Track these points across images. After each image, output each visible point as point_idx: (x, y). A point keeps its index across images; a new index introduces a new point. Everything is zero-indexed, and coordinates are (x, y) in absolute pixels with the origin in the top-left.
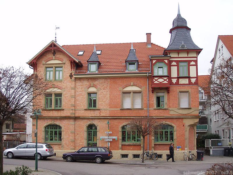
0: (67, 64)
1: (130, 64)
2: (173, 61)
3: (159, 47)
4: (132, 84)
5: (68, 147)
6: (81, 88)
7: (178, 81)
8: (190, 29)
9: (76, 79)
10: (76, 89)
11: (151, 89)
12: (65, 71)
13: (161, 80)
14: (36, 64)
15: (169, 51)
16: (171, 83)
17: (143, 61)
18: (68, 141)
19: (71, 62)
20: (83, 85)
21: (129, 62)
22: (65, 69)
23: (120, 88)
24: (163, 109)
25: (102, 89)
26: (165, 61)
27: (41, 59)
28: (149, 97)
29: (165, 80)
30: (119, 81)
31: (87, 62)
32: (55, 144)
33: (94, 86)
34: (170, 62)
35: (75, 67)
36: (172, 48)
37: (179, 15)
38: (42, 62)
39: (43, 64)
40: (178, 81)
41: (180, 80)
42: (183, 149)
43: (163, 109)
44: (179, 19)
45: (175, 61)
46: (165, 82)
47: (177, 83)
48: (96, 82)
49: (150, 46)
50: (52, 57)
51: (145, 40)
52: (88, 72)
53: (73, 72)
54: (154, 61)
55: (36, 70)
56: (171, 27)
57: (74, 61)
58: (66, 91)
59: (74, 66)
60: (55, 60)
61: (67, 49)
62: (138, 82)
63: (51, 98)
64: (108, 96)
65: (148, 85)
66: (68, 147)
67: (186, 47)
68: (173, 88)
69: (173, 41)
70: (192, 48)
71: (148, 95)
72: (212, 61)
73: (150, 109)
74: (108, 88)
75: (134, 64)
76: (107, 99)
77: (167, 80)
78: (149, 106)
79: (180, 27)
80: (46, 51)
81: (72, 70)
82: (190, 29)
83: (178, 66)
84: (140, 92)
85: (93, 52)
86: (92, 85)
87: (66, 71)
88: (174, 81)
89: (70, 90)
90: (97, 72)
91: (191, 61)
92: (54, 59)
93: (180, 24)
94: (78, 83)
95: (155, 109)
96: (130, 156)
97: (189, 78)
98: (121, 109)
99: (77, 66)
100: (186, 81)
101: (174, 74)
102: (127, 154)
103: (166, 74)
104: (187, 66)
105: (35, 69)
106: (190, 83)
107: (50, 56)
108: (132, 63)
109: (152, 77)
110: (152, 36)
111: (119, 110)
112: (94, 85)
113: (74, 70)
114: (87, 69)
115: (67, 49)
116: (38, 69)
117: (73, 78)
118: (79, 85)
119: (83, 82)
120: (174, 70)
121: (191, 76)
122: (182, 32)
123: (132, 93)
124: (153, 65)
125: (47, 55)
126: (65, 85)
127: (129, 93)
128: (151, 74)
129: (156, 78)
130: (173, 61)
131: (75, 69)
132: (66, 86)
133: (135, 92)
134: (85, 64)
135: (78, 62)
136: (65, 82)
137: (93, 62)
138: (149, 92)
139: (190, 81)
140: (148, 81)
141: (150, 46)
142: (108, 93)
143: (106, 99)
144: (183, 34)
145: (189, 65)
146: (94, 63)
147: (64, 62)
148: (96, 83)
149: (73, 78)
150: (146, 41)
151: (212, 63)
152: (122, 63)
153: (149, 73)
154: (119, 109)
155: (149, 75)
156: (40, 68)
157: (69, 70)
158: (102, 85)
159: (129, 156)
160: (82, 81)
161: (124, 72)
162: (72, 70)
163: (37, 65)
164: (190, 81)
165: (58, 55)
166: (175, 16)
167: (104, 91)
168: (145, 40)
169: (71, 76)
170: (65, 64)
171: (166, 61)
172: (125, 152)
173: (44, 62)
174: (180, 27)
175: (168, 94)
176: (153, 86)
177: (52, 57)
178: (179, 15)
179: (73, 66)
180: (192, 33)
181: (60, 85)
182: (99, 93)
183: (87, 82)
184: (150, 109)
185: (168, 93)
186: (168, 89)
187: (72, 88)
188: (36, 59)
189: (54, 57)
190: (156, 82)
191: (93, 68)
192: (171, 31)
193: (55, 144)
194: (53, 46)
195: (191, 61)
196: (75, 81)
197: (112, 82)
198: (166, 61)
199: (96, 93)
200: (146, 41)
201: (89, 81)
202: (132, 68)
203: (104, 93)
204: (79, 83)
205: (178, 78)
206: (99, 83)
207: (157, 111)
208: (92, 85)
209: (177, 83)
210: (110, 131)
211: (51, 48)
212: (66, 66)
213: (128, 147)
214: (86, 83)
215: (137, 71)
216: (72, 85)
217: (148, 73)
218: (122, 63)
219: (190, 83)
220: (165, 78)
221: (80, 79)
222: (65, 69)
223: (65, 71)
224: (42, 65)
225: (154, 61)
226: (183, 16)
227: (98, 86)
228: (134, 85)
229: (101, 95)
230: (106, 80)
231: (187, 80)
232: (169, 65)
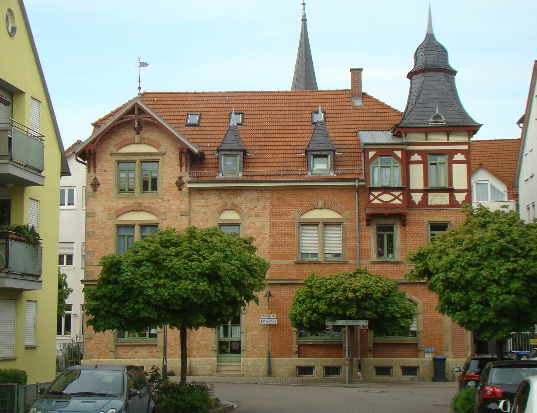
0: (315, 304)
1: (315, 156)
2: (413, 152)
3: (383, 104)
4: (321, 203)
5: (173, 352)
6: (202, 211)
7: (425, 199)
8: (454, 73)
9: (192, 192)
10: (192, 214)
11: (363, 216)
12: (164, 170)
13: (386, 197)
14: (95, 153)
15: (406, 130)
16: (409, 203)
17: (345, 147)
18: (174, 337)
19: (181, 153)
20: (207, 206)
21: (313, 153)
22: (165, 167)
23: (294, 214)
24: (392, 263)
25: (252, 214)
26: (396, 155)
27: (107, 141)
28: (360, 235)
29: (396, 198)
30: (290, 197)
31: (218, 151)
32: (141, 346)
33: (234, 208)
34: (408, 154)
35: (189, 163)
36: (411, 122)
37: (430, 37)
38: (107, 148)
39: (112, 155)
40: (425, 199)
41: (431, 196)
42: (357, 357)
43: (392, 263)
44: (428, 49)
45: (419, 152)
46: (397, 202)
47: (424, 203)
48: (239, 198)
49: (358, 103)
50: (134, 138)
51: (346, 84)
52: (220, 175)
53: (187, 178)
54: (371, 154)
55: (95, 167)
56: (410, 67)
57: (190, 152)
58: (168, 220)
59: (186, 161)
60: (141, 143)
61: (156, 106)
62: (335, 199)
63: (132, 234)
64: (267, 231)
65: (359, 207)
66: (173, 352)
67: (443, 121)
68: (413, 215)
69: (414, 99)
70: (458, 121)
71: (357, 230)
72: (521, 121)
73: (362, 262)
74: (267, 212)
75: (326, 156)
76: (264, 239)
77: (401, 197)
78: (362, 254)
79: (432, 66)
80: (118, 122)
81: (181, 170)
82: (454, 73)
83: (424, 162)
84: (338, 223)
85: (227, 128)
86: (229, 206)
87: (168, 171)
88: (417, 198)
89: (177, 217)
90: (241, 175)
91: (456, 152)
92: (139, 142)
93: (432, 60)
94: (196, 201)
95: (374, 263)
96: (318, 371)
97: (451, 191)
98: (297, 263)
99: (194, 160)
100: (443, 199)
101: (417, 181)
102: (311, 365)
103: (398, 183)
104: (447, 164)
105: (92, 166)
106: (453, 204)
107: (129, 134)
108: (320, 155)
109: (365, 190)
110: (364, 75)
111: (293, 263)
112: (233, 205)
113: (186, 171)
114: (217, 167)
115: (156, 106)
116: (99, 166)
117: (185, 190)
118: (199, 204)
119: (207, 199)
120: (417, 173)
121: (455, 186)
122: (435, 83)
123: (320, 225)
124: (368, 162)
125: (121, 132)
126: (166, 204)
127: (314, 223)
128: (363, 183)
129: (376, 193)
130: (413, 152)
131: (188, 168)
132: (169, 208)
133: (328, 224)
134: (210, 155)
135: (196, 151)
136: (167, 197)
137: (231, 152)
138: (359, 223)
139: (452, 198)
140: (358, 198)
141: (358, 103)
142: (267, 225)
143: (262, 238)
144: (438, 87)
145: (451, 162)
146: (234, 153)
147: (162, 149)
148: (239, 200)
149: (185, 190)
150: (349, 87)
151: (521, 125)
152: (295, 152)
153: (359, 181)
154: (292, 262)
155: (359, 185)
156: (105, 164)
157: (176, 169)
158: (252, 207)
159: (315, 372)
160: (206, 195)
161: (302, 178)
162: (181, 170)
163: (98, 156)
164: (452, 198)
165: (146, 134)
166: (421, 39)
167: (256, 219)
168: (346, 84)
169: (180, 184)
170: (164, 154)
171: (399, 154)
172: (304, 362)
173: (113, 150)
174: (432, 66)
175: (404, 227)
176: (370, 211)
177: (133, 136)
178: (430, 37)
179: (184, 159)
180: (457, 79)
181: (154, 204)
182: (245, 224)
183: (217, 198)
184: (362, 262)
185: (404, 225)
186: (403, 218)
187: (182, 212)
188: (95, 144)
189: (137, 138)
190: (376, 202)
191: (231, 166)
192: (410, 76)
193: (141, 346)
194: (136, 112)
195: (456, 152)
196: (189, 196)
197: (276, 199)
198: (399, 154)
199: (238, 225)
200: (349, 87)
201: (222, 195)
202: (321, 166)
203: (257, 223)
204: (198, 201)
205: (426, 191)
206: (245, 202)
207: (377, 267)
208: (229, 206)
209: (424, 203)
210: (271, 313)
211: (133, 117)
212: (168, 160)
213: (312, 350)
214: (214, 201)
215: (332, 174)
216: (181, 204)
217: (357, 181)
218: (295, 152)
219: (453, 204)
220: (397, 193)
221: (201, 192)
222: (165, 167)
223: (163, 172)
224: (108, 157)
225: (371, 154)
226: (440, 38)
227: (243, 208)
228: (325, 207)
229: (251, 230)
230: (260, 194)
231: (446, 196)
232: (406, 163)
